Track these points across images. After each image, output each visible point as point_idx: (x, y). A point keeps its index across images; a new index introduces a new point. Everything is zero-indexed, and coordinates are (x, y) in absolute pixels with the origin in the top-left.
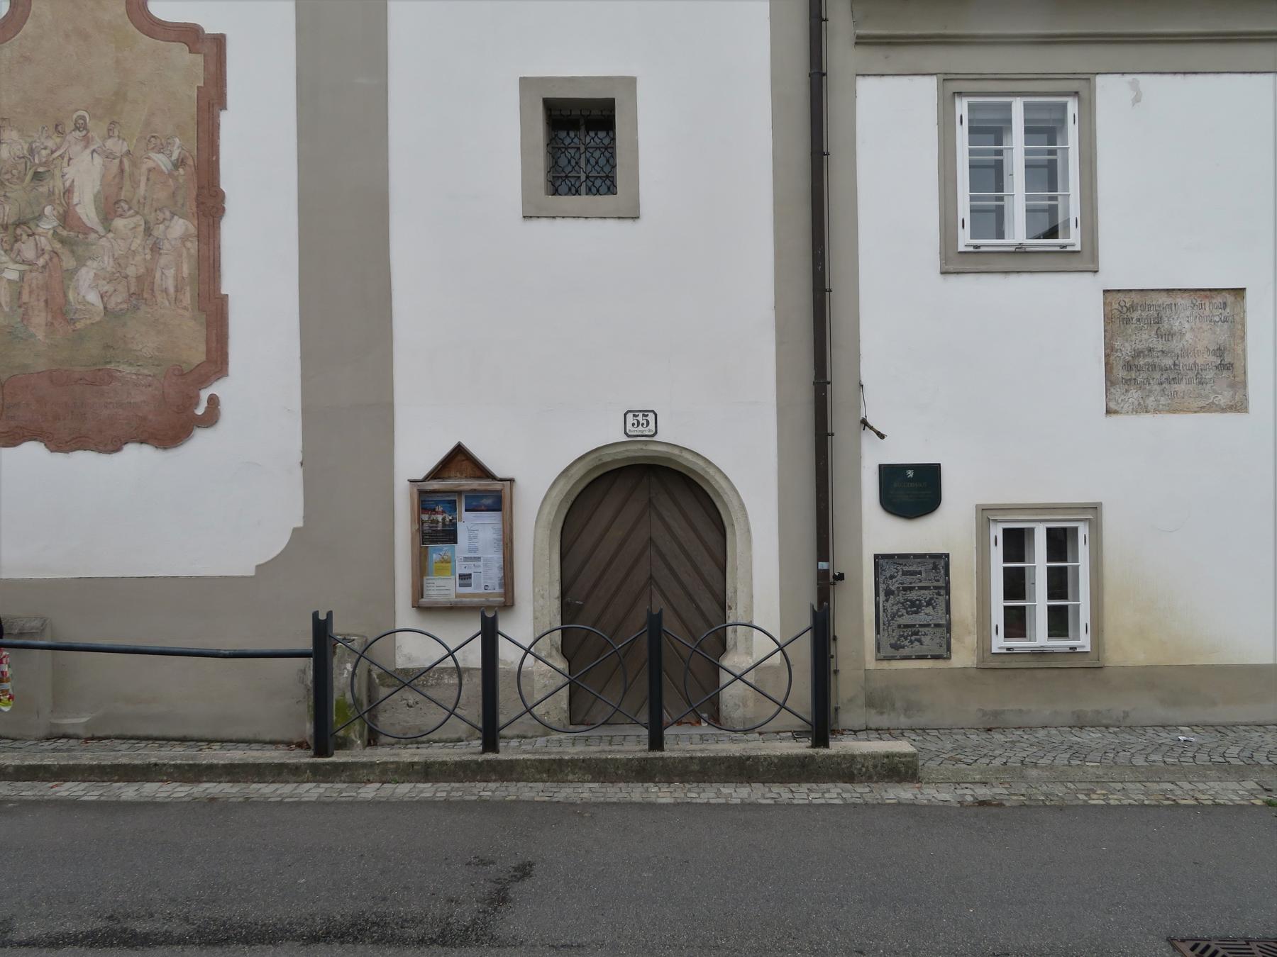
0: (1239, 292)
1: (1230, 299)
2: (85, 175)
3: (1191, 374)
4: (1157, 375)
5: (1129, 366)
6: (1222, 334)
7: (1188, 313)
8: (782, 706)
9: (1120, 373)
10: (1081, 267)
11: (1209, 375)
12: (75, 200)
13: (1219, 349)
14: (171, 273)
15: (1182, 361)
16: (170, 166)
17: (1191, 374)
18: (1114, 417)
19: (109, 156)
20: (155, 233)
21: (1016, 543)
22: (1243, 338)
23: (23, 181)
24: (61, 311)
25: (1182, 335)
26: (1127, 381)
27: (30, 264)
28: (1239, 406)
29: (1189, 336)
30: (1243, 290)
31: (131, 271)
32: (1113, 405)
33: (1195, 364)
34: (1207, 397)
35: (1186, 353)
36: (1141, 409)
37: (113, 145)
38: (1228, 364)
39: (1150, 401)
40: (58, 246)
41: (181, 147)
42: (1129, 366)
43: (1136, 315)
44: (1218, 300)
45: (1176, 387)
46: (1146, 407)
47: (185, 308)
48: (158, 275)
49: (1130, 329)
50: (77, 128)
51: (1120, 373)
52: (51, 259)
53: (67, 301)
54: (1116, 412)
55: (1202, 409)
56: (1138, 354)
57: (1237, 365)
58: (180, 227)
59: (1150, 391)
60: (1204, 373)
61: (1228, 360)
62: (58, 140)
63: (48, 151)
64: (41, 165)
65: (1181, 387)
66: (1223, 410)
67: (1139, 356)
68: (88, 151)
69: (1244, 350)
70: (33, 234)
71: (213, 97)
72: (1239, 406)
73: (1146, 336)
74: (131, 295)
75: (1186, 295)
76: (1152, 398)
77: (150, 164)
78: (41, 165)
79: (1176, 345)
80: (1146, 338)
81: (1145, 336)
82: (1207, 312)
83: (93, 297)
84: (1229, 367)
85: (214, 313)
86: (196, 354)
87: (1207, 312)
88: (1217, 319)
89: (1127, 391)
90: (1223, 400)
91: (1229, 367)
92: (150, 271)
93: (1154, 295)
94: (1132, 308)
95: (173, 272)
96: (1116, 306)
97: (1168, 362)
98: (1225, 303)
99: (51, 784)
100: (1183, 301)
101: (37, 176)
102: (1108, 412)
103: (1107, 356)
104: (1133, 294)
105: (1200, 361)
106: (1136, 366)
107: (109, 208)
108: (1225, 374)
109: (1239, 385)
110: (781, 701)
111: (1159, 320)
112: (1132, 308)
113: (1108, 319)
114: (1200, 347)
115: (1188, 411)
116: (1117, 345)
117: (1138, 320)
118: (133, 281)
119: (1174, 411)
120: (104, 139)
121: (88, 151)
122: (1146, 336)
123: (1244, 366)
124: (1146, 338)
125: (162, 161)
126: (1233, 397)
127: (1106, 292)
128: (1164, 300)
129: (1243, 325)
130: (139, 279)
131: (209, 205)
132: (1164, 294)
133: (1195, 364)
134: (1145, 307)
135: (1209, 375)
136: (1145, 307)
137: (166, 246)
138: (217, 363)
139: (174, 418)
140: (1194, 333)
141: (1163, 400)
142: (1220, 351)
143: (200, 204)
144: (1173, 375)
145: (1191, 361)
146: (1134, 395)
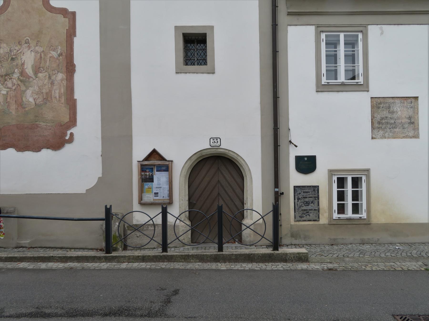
0: (416, 98)
1: (413, 100)
2: (28, 59)
3: (400, 126)
4: (389, 126)
5: (379, 123)
6: (411, 112)
7: (399, 105)
8: (263, 237)
9: (376, 125)
10: (363, 90)
11: (406, 126)
12: (25, 67)
13: (410, 117)
14: (57, 91)
15: (397, 121)
16: (57, 56)
17: (400, 126)
18: (374, 140)
19: (37, 52)
20: (52, 78)
21: (341, 182)
22: (418, 113)
23: (8, 61)
24: (20, 104)
25: (397, 112)
26: (379, 128)
27: (10, 88)
28: (416, 136)
29: (399, 113)
30: (418, 97)
31: (44, 91)
32: (374, 136)
33: (401, 122)
34: (406, 133)
35: (398, 118)
36: (383, 137)
37: (38, 49)
38: (413, 122)
39: (386, 135)
40: (19, 82)
41: (61, 49)
42: (379, 123)
43: (381, 106)
44: (409, 101)
45: (395, 130)
46: (385, 137)
47: (62, 103)
48: (53, 92)
49: (380, 110)
50: (26, 43)
51: (376, 125)
52: (17, 87)
53: (22, 101)
54: (375, 138)
55: (404, 137)
56: (382, 119)
57: (416, 122)
58: (60, 76)
59: (386, 131)
60: (404, 125)
61: (412, 121)
62: (20, 47)
63: (16, 51)
64: (14, 55)
65: (397, 130)
66: (411, 138)
67: (382, 119)
68: (30, 51)
69: (418, 118)
70: (11, 79)
71: (71, 33)
72: (416, 136)
73: (385, 113)
74: (44, 99)
75: (398, 99)
76: (387, 134)
77: (51, 55)
78: (14, 55)
79: (395, 116)
80: (385, 113)
81: (385, 113)
82: (406, 105)
83: (31, 100)
84: (413, 123)
85: (72, 105)
86: (66, 119)
87: (406, 105)
88: (409, 107)
89: (379, 131)
90: (411, 134)
91: (413, 123)
92: (50, 91)
93: (388, 99)
94: (380, 103)
95: (58, 91)
96: (375, 103)
97: (392, 121)
98: (411, 102)
99: (17, 263)
100: (397, 101)
101: (13, 59)
102: (372, 138)
103: (372, 119)
104: (381, 99)
105: (403, 121)
106: (382, 123)
107: (37, 70)
108: (412, 125)
109: (416, 129)
110: (262, 235)
111: (389, 107)
112: (380, 103)
113: (372, 107)
114: (403, 117)
115: (399, 138)
116: (375, 116)
117: (382, 107)
118: (45, 94)
119: (395, 138)
120: (35, 47)
121: (30, 51)
122: (385, 113)
123: (418, 123)
124: (385, 113)
125: (54, 54)
126: (414, 133)
127: (371, 98)
128: (391, 100)
129: (418, 109)
130: (47, 93)
131: (70, 69)
132: (391, 99)
133: (401, 122)
134: (385, 103)
135: (406, 126)
136: (385, 103)
137: (56, 83)
138: (73, 122)
139: (58, 140)
140: (401, 112)
141: (391, 134)
142: (410, 118)
143: (67, 68)
144: (394, 126)
145: (400, 121)
146: (381, 132)
